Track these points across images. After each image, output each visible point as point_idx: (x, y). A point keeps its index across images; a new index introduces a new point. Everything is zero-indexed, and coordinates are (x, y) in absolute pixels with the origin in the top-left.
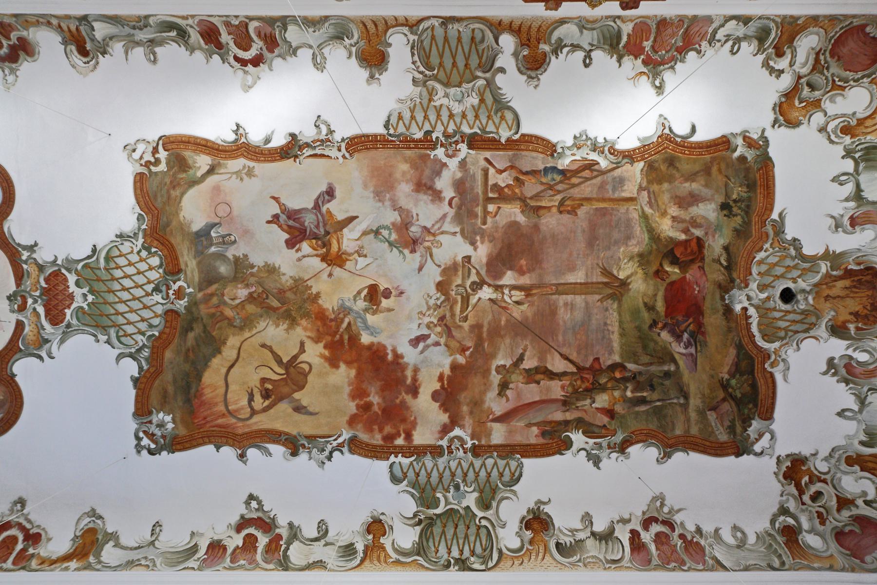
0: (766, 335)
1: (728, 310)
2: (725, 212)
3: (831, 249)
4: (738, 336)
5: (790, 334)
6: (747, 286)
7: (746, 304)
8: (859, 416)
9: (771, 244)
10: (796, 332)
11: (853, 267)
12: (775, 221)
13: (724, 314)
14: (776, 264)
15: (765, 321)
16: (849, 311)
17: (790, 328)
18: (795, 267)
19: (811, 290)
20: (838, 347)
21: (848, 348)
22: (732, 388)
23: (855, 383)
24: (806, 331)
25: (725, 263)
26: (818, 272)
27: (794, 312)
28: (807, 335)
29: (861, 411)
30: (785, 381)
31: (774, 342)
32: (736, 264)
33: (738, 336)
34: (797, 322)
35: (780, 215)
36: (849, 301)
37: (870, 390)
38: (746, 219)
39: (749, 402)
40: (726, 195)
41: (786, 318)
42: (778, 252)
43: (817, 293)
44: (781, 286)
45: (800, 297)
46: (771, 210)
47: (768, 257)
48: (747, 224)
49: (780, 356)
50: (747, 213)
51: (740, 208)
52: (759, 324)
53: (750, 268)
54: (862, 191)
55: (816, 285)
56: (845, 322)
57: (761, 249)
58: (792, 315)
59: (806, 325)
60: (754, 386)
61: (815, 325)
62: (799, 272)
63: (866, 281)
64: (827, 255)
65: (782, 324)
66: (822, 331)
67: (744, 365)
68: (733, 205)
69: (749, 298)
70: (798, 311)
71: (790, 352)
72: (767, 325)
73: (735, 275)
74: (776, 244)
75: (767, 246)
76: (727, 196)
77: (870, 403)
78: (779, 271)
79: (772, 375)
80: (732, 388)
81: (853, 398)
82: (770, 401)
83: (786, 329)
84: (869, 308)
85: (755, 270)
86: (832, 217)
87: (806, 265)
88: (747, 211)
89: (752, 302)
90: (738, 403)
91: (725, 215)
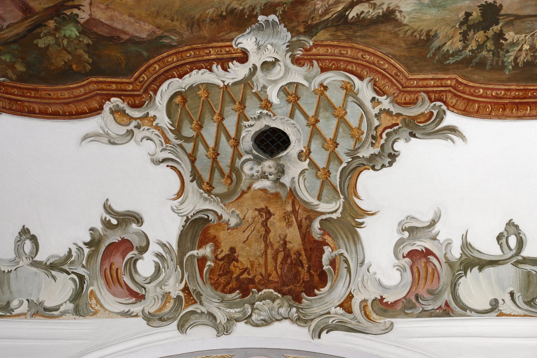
0: (185, 100)
1: (242, 21)
2: (476, 14)
3: (367, 220)
4: (180, 43)
5: (189, 147)
6: (297, 61)
7: (255, 59)
8: (24, 262)
9: (388, 112)
10: (193, 158)
11: (327, 254)
12: (441, 117)
13: (232, 12)
14: (342, 119)
15: (216, 98)
16: (239, 248)
17: (201, 147)
18: (334, 157)
19: (283, 185)
20: (163, 227)
21: (163, 245)
22: (57, 29)
23: (90, 256)
24: (196, 176)
25: (352, 14)
26: (319, 199)
27: (237, 154)
28: (187, 178)
29: (36, 264)
30: (85, 138)
31: (169, 115)
32: (349, 39)
33: (180, 43)
34: (215, 160)
35: (453, 130)
36: (258, 247)
37: (81, 278)
38: (452, 60)
39: (28, 65)
40: (518, 17)
41: (223, 138)
42: (369, 124)
43: (277, 195)
44: (296, 133)
45: (269, 165)
46: (465, 113)
47: (361, 105)
48: (442, 62)
49: (138, 127)
50: (466, 62)
51: (480, 47)
52: (208, 86)
53: (338, 69)
54: (480, 270)
55: (292, 194)
56: (215, 241)
57: (380, 91)
58: (230, 150)
59: (209, 175)
60: (66, 75)
61: (209, 192)
62: (321, 164)
63: (298, 273)
64: (353, 217)
65: (209, 132)
66: (195, 202)
67: (116, 53)
68: (490, 33)
69: (268, 66)
70: (238, 163)
71: (150, 146)
72: (206, 102)
73: (323, 35)
74: (387, 121)
75: (385, 103)
76: (515, 19)
77: (54, 278)
78: (328, 126)
79: (98, 110)
80: (57, 29)
81: (63, 253)
82: (36, 107)
83: (198, 138)
84: (245, 276)
85: (332, 78)
86: (433, 223)
87: (336, 178)
88: (471, 63)
89: (259, 73)
90: (25, 41)
91: (468, 14)
